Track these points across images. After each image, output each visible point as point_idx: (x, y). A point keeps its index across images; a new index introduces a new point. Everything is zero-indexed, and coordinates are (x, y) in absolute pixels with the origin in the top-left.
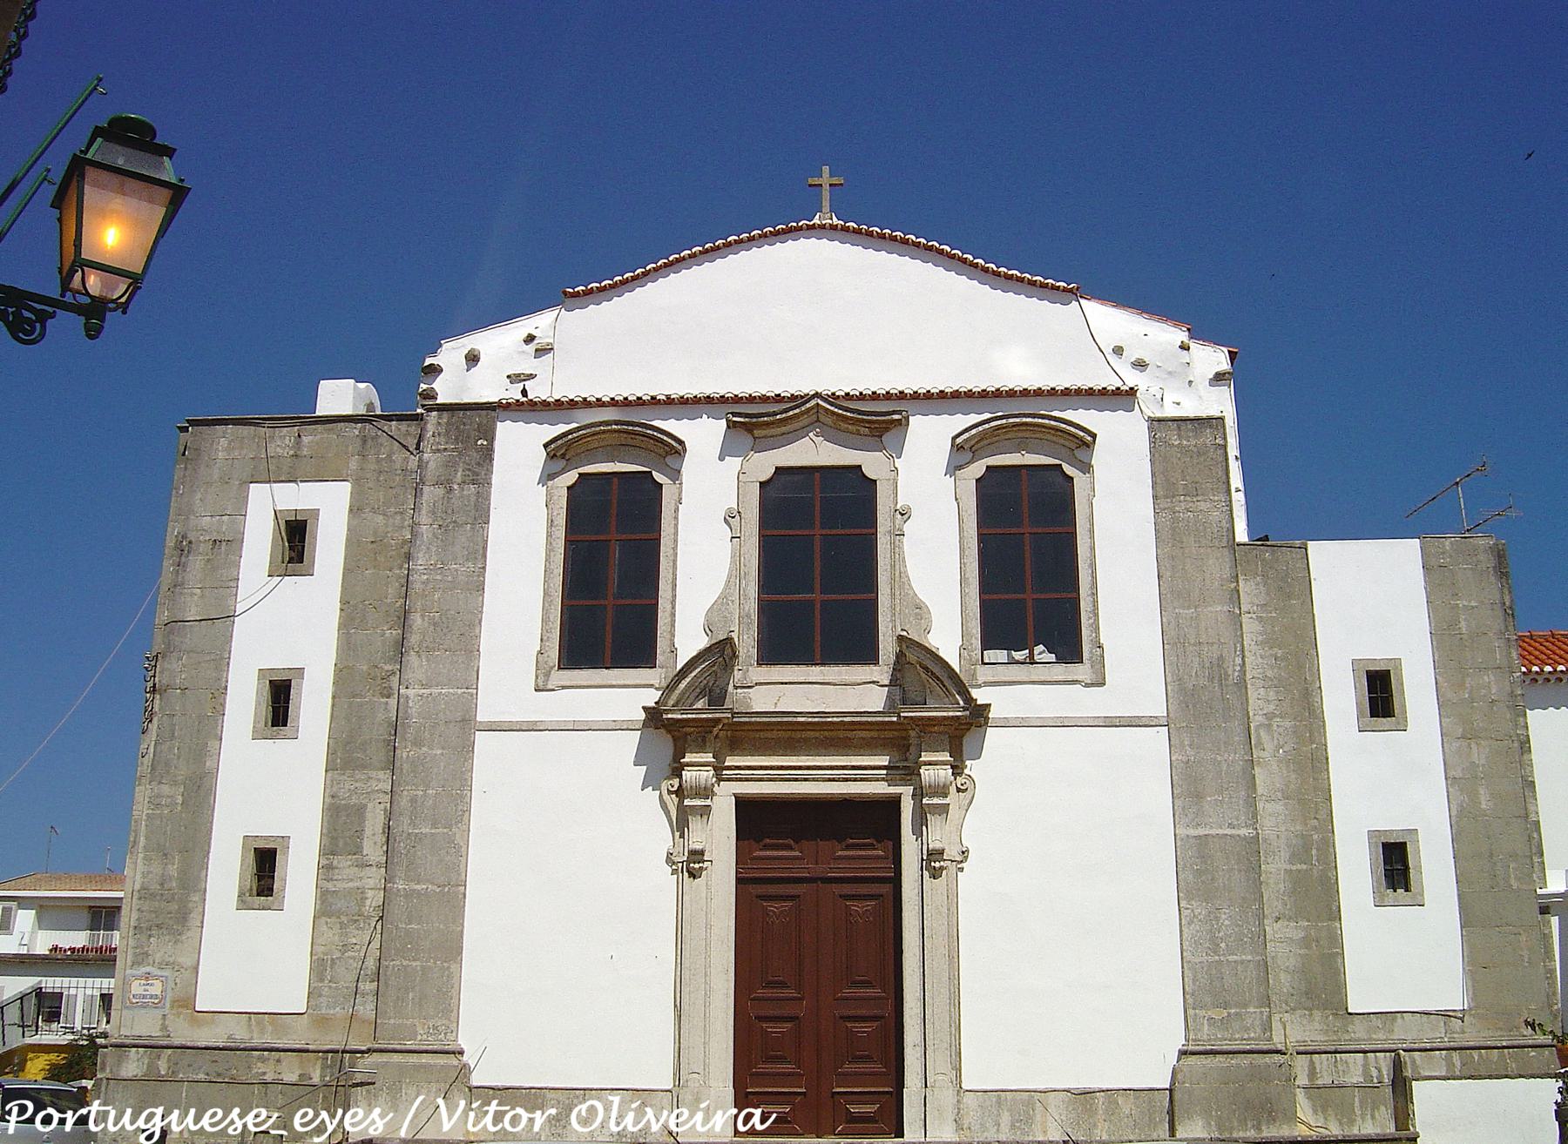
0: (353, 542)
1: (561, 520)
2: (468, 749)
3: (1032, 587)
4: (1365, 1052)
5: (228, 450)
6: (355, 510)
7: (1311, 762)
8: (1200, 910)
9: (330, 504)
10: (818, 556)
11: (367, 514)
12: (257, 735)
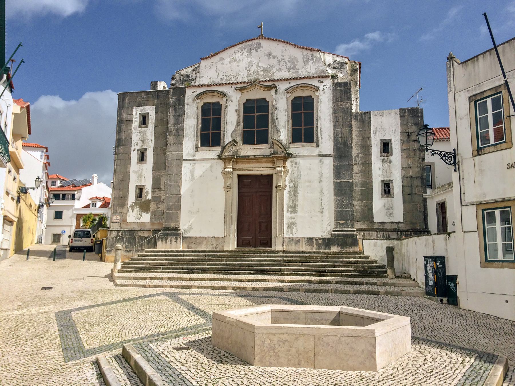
0: (156, 119)
1: (200, 114)
2: (181, 166)
3: (304, 129)
4: (377, 231)
5: (129, 100)
6: (156, 113)
7: (367, 164)
8: (339, 198)
9: (151, 110)
10: (256, 120)
11: (159, 114)
12: (138, 163)
